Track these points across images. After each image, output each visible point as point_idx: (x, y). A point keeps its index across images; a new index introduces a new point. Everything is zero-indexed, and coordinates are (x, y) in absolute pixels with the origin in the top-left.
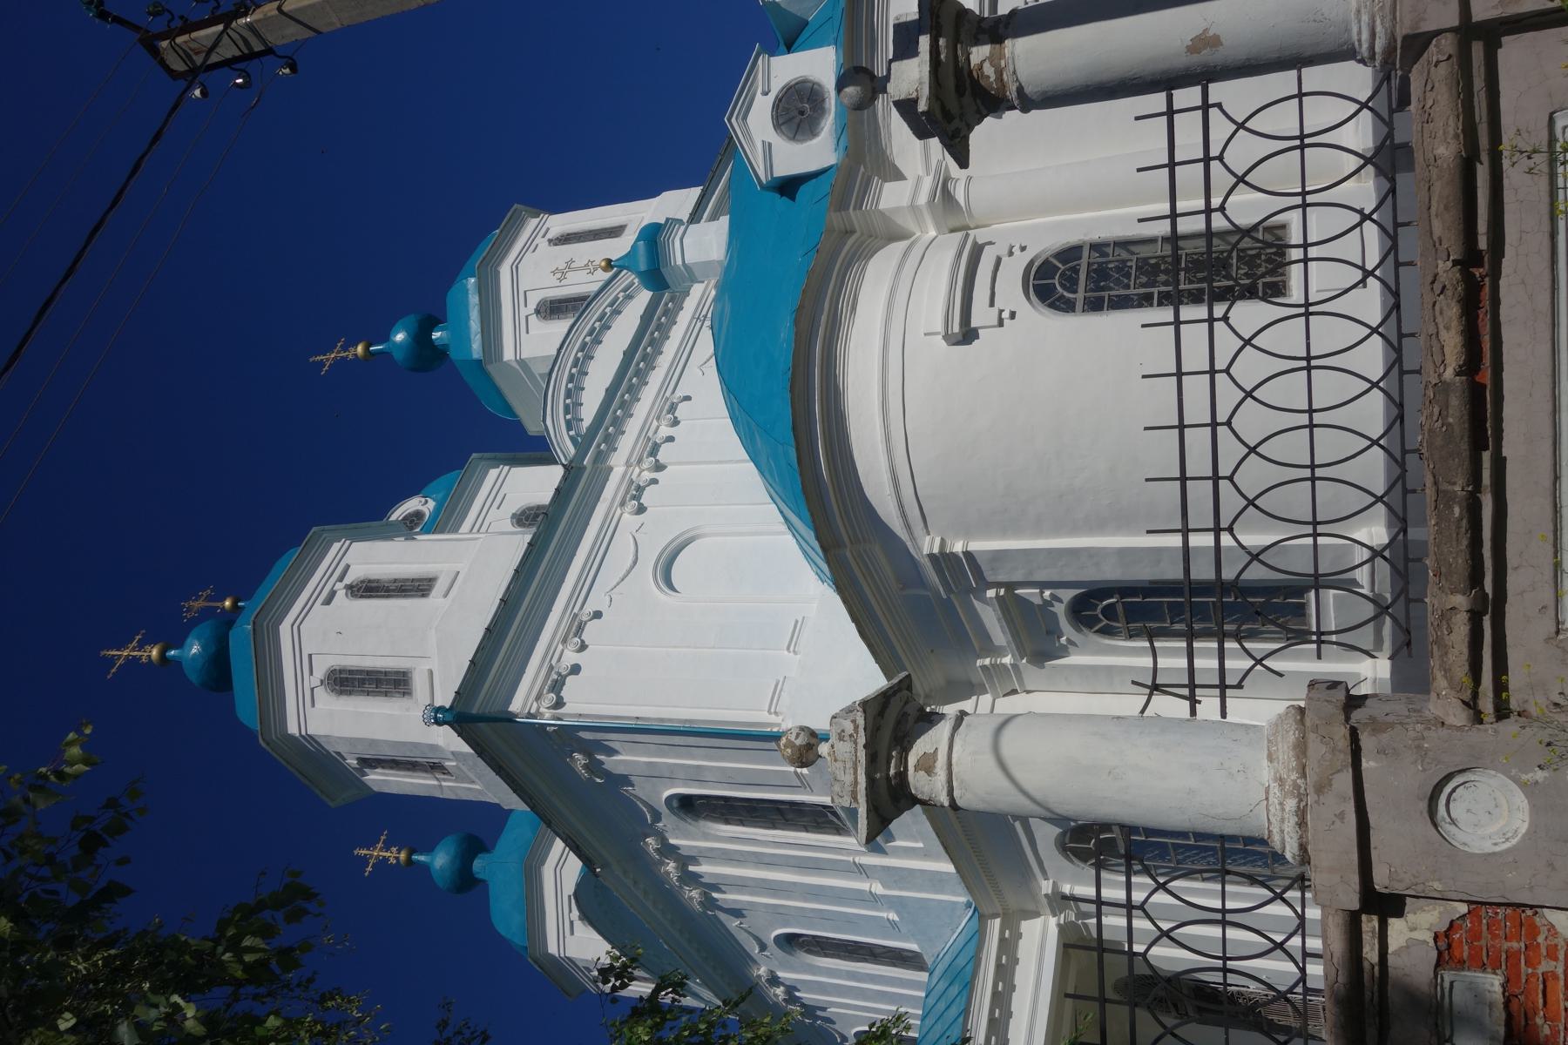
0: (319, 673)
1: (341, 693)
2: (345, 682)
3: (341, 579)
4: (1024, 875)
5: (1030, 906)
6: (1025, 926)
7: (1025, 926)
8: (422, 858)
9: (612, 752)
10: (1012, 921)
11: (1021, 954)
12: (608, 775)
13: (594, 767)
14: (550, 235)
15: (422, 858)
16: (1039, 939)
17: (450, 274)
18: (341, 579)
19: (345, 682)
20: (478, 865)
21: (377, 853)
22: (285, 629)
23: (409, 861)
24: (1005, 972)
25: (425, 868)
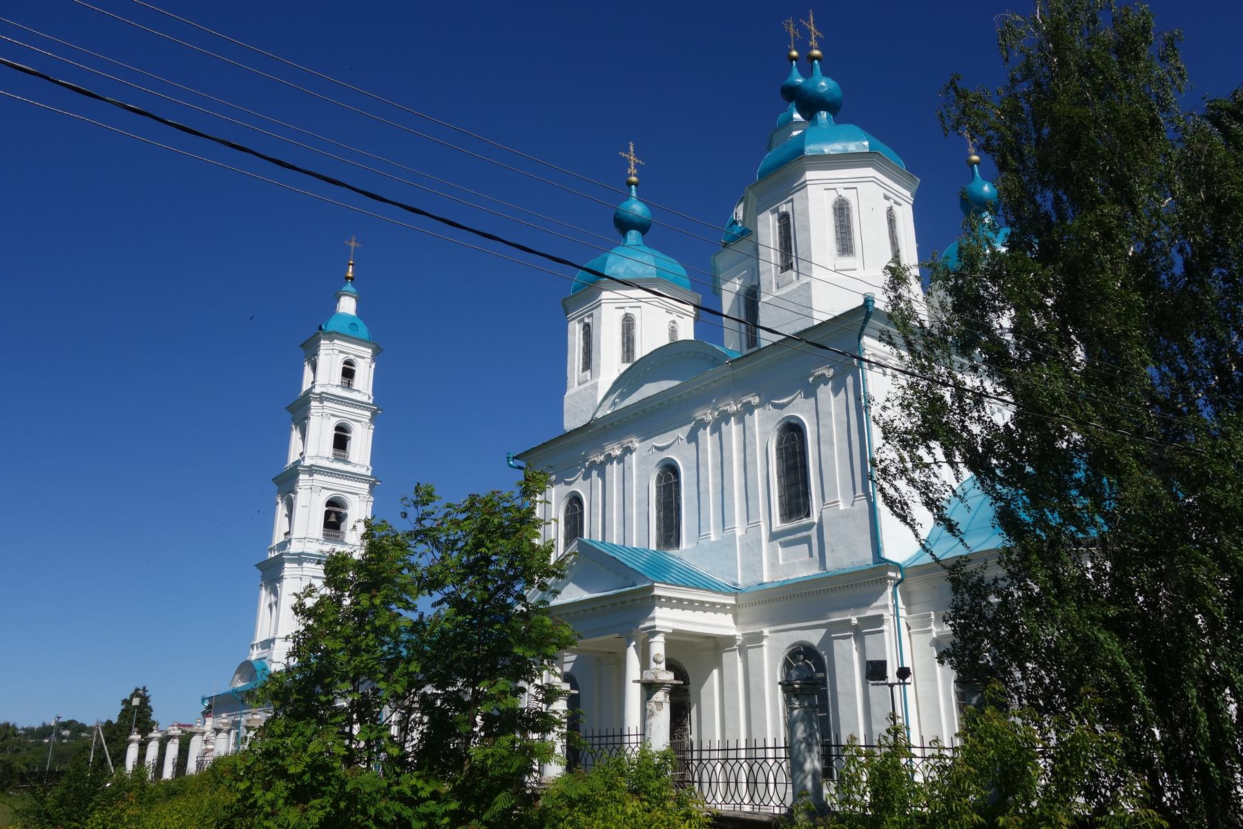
0: (847, 195)
1: (835, 209)
2: (842, 210)
3: (896, 202)
4: (776, 619)
5: (740, 620)
6: (730, 616)
7: (730, 616)
8: (634, 193)
9: (836, 392)
10: (734, 610)
11: (719, 615)
12: (816, 385)
13: (822, 379)
14: (895, 207)
15: (634, 193)
16: (721, 624)
17: (871, 128)
18: (896, 202)
19: (842, 210)
20: (633, 236)
21: (633, 159)
22: (870, 172)
23: (630, 184)
24: (701, 606)
25: (627, 196)
